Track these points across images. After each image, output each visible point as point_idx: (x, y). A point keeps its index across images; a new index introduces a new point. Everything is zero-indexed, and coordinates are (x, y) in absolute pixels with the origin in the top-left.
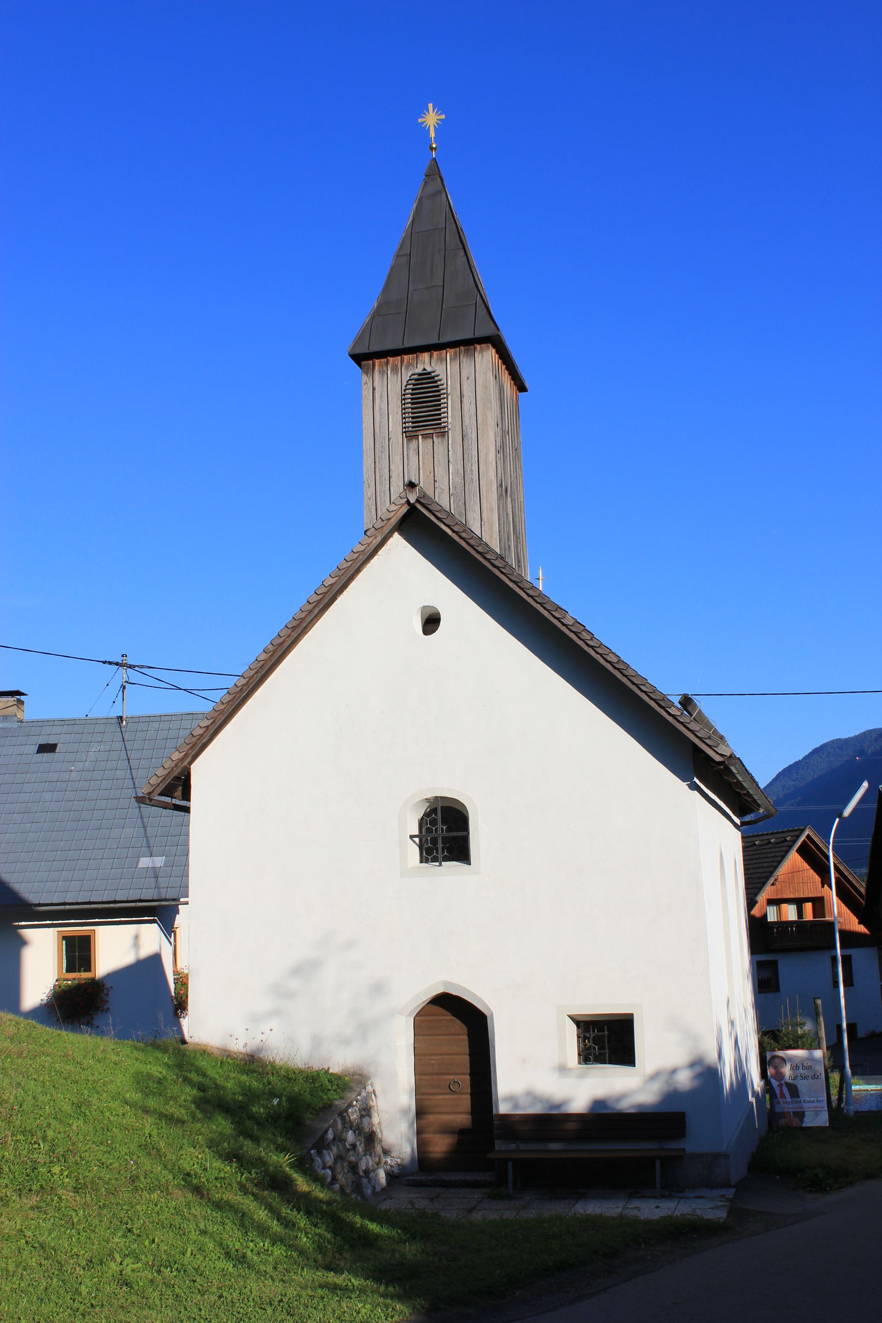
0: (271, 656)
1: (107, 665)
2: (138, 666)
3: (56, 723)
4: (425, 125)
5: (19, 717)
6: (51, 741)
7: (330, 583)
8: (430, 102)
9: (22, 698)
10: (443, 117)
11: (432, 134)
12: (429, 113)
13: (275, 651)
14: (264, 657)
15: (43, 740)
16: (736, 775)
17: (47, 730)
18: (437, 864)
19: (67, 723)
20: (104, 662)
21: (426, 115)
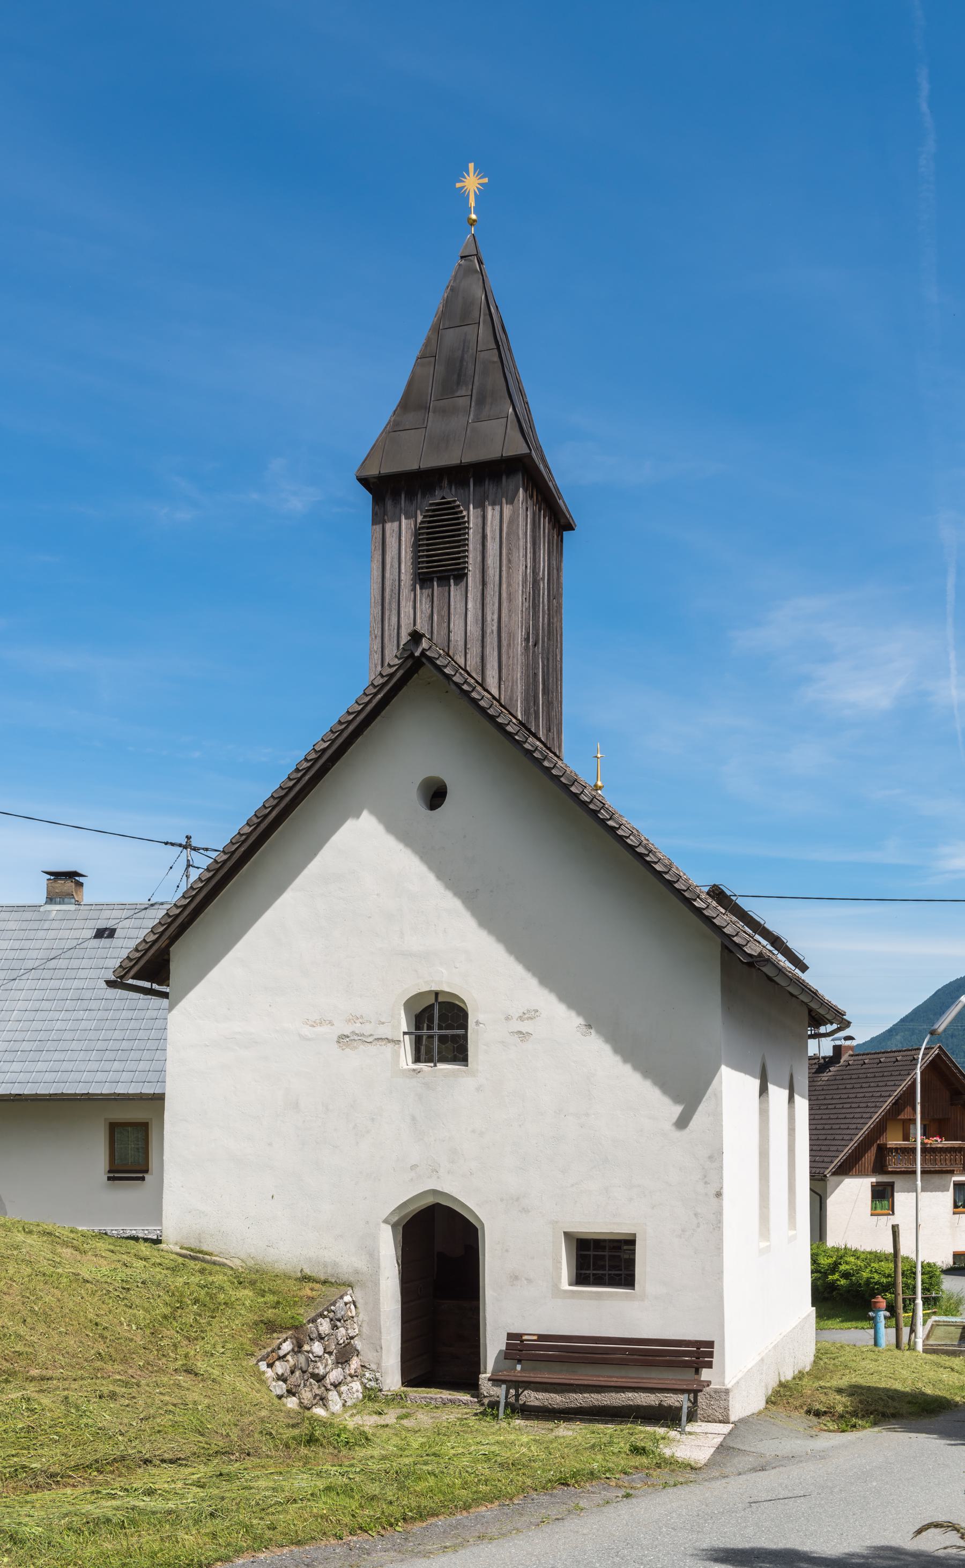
0: (255, 829)
1: (169, 846)
2: (203, 849)
3: (116, 907)
4: (480, 187)
5: (77, 899)
6: (110, 924)
7: (322, 747)
8: (471, 162)
9: (81, 879)
10: (486, 180)
11: (472, 203)
12: (469, 176)
13: (259, 824)
14: (247, 830)
15: (102, 924)
16: (787, 988)
17: (106, 914)
18: (432, 1064)
19: (127, 907)
20: (166, 843)
21: (477, 176)
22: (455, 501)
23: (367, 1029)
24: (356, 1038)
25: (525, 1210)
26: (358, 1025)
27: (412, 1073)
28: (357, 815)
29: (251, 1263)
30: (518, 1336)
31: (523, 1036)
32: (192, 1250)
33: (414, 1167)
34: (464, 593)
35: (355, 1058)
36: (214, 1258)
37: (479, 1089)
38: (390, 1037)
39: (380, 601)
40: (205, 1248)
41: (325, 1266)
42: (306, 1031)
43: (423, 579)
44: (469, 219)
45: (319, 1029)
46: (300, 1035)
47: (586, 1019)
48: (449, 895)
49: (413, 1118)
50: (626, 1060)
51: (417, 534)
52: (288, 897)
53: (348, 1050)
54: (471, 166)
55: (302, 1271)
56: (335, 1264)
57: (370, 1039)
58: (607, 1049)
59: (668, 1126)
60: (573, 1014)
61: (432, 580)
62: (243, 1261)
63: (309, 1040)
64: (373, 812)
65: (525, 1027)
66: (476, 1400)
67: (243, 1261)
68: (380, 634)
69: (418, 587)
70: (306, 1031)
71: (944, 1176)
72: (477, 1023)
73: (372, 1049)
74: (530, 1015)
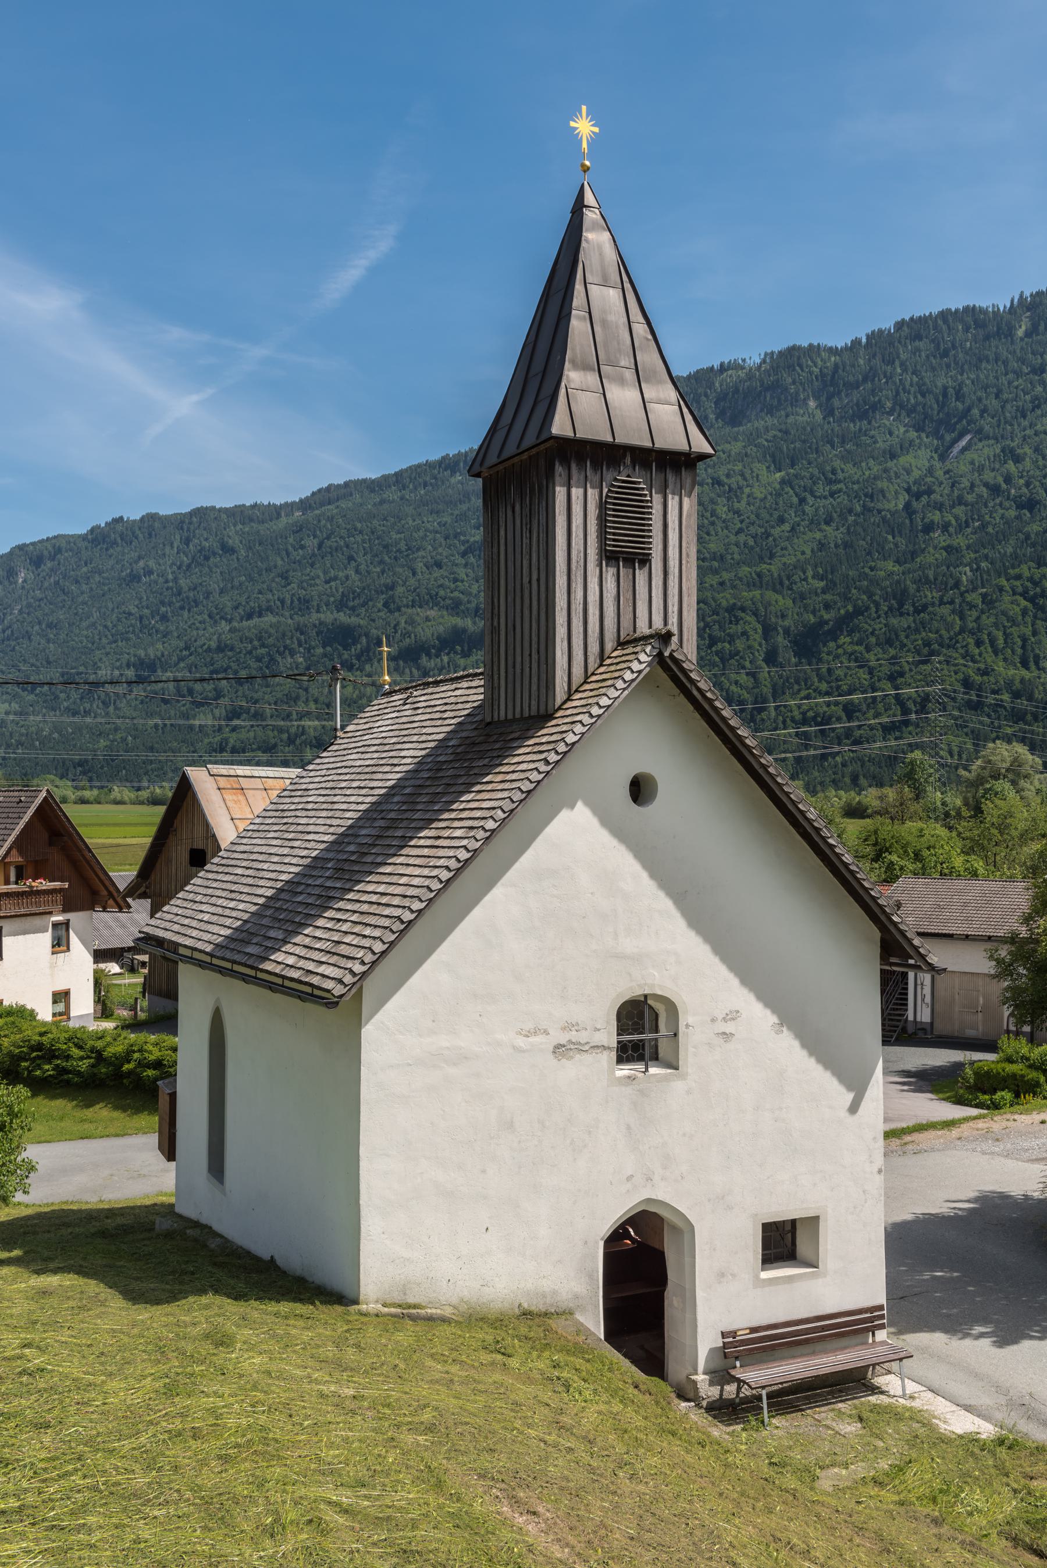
22: (639, 483)
23: (583, 1037)
24: (572, 1047)
25: (730, 1208)
26: (574, 1033)
27: (627, 1080)
28: (572, 807)
29: (463, 1308)
30: (734, 1334)
31: (726, 1036)
32: (400, 1306)
33: (630, 1178)
34: (647, 578)
35: (572, 1069)
36: (429, 1311)
37: (689, 1092)
38: (606, 1045)
39: (565, 571)
40: (411, 1300)
41: (544, 1296)
42: (521, 1042)
43: (609, 556)
44: (583, 165)
45: (533, 1039)
46: (514, 1047)
47: (780, 1017)
48: (661, 894)
49: (629, 1127)
50: (811, 1053)
51: (602, 506)
52: (498, 892)
53: (564, 1060)
54: (584, 108)
55: (520, 1305)
56: (555, 1292)
57: (586, 1048)
58: (796, 1044)
59: (843, 1113)
60: (768, 1012)
61: (617, 560)
62: (455, 1307)
63: (524, 1051)
64: (587, 803)
65: (729, 1027)
66: (693, 1404)
67: (455, 1307)
68: (565, 606)
69: (604, 563)
70: (521, 1042)
71: (44, 916)
72: (687, 1026)
73: (588, 1058)
74: (732, 1016)
